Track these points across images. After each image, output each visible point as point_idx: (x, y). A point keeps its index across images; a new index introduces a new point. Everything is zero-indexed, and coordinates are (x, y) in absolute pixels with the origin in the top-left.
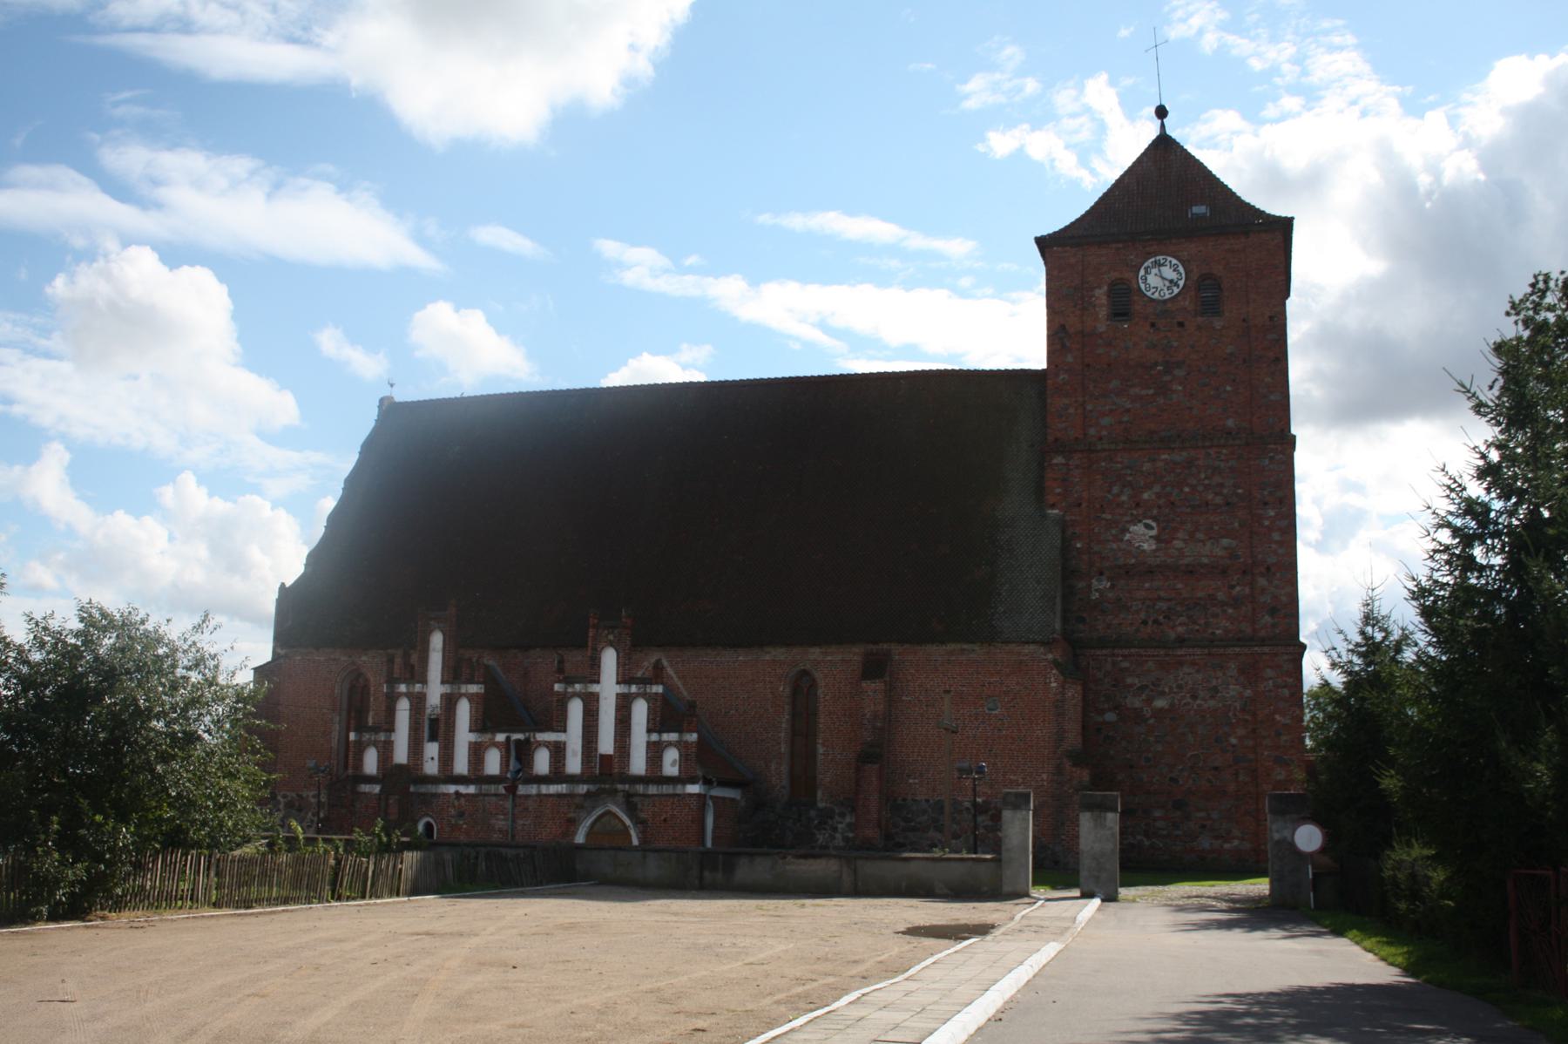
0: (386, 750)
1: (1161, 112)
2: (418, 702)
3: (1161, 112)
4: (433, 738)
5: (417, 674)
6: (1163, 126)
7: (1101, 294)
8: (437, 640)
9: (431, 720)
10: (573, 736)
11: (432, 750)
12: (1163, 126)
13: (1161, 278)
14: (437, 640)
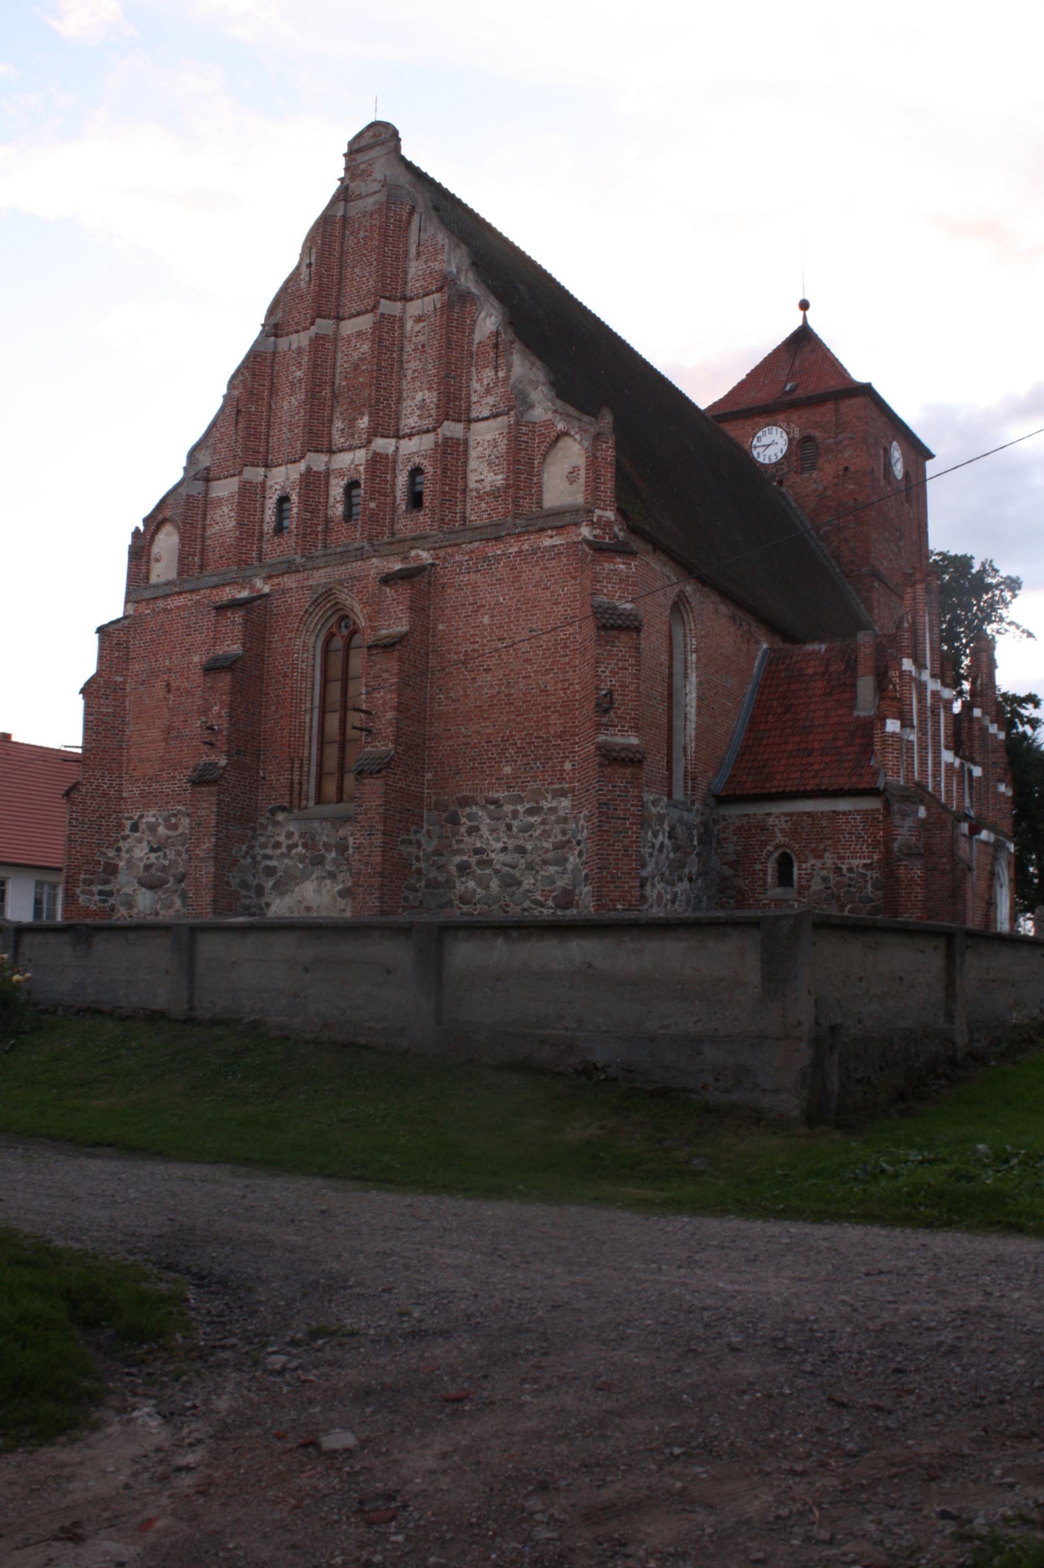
1: (804, 305)
3: (804, 305)
6: (805, 318)
12: (805, 318)
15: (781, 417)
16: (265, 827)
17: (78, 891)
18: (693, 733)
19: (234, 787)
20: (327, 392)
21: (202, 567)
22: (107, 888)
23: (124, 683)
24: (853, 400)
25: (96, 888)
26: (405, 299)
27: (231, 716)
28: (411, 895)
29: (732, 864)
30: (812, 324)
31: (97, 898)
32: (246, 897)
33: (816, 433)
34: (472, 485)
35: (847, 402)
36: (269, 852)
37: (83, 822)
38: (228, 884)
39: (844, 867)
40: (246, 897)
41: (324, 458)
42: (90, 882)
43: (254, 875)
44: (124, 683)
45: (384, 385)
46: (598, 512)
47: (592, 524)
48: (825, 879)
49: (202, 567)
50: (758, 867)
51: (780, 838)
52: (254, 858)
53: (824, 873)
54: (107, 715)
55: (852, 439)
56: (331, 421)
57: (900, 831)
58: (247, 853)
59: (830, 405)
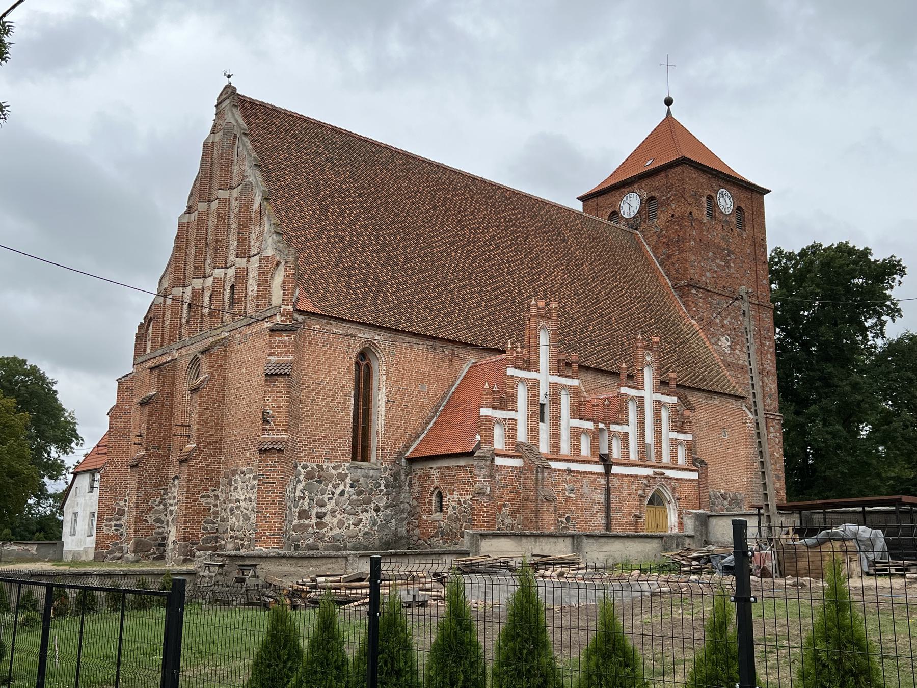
0: (512, 425)
1: (669, 102)
2: (534, 386)
3: (669, 102)
4: (542, 405)
5: (529, 364)
6: (669, 112)
7: (704, 199)
8: (544, 339)
9: (542, 421)
10: (631, 429)
11: (544, 429)
12: (669, 112)
13: (726, 202)
14: (544, 339)
15: (636, 186)
16: (171, 488)
17: (103, 525)
18: (383, 422)
19: (151, 467)
20: (203, 245)
21: (162, 344)
22: (119, 523)
23: (130, 409)
24: (676, 169)
25: (113, 523)
26: (231, 188)
27: (148, 428)
28: (209, 526)
29: (416, 498)
30: (675, 115)
31: (113, 528)
32: (159, 527)
33: (656, 194)
34: (250, 293)
35: (673, 170)
36: (171, 502)
37: (107, 487)
38: (146, 521)
39: (462, 500)
40: (159, 527)
41: (201, 280)
42: (110, 520)
43: (166, 515)
44: (130, 409)
45: (220, 239)
46: (283, 307)
47: (282, 315)
48: (454, 508)
49: (162, 344)
50: (427, 500)
51: (436, 483)
52: (165, 505)
53: (454, 504)
54: (121, 427)
55: (675, 195)
56: (205, 260)
57: (478, 478)
58: (160, 503)
59: (663, 174)
